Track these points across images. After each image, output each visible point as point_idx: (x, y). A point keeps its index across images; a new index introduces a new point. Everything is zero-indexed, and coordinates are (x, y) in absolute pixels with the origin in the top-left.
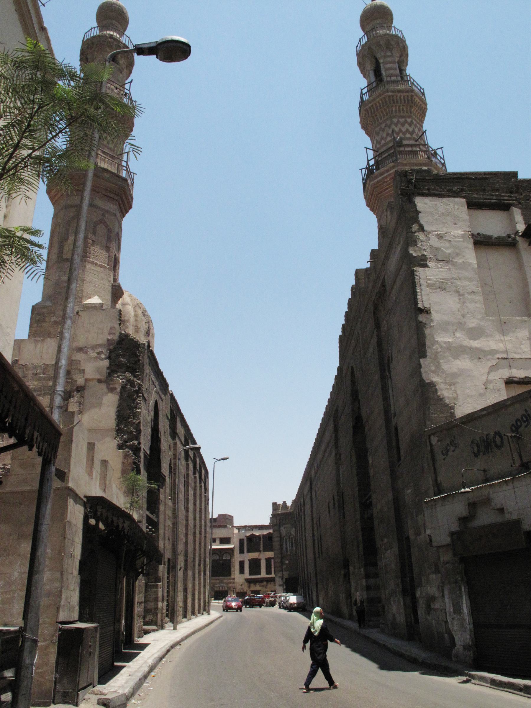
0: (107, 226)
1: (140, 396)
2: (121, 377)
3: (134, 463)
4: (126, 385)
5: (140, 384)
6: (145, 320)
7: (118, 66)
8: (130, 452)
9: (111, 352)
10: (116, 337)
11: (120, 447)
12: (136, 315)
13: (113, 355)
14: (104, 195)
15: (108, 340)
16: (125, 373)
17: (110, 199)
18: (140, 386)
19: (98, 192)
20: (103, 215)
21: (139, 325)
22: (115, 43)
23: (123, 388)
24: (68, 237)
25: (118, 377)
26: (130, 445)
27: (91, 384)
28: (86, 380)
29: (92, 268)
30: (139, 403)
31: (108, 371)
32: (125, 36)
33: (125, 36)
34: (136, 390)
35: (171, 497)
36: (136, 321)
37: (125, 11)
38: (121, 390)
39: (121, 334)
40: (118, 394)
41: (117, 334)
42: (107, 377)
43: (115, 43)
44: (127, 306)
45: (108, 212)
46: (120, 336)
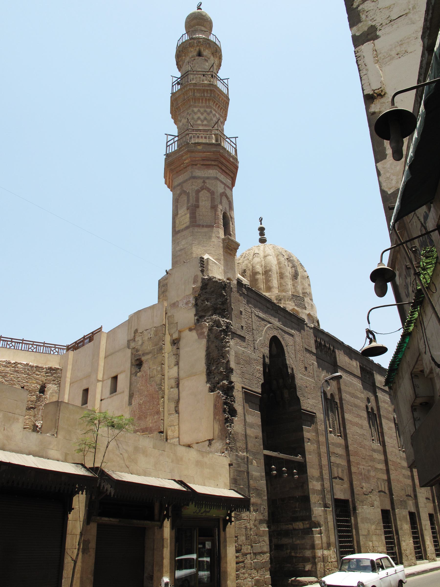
0: (209, 190)
1: (229, 334)
2: (207, 321)
3: (225, 403)
4: (213, 326)
5: (228, 323)
6: (291, 265)
7: (203, 58)
8: (221, 393)
9: (196, 299)
10: (199, 284)
11: (212, 390)
12: (279, 263)
13: (199, 302)
14: (202, 165)
15: (193, 288)
16: (212, 315)
17: (208, 166)
18: (228, 325)
19: (196, 165)
20: (204, 182)
21: (283, 271)
22: (195, 42)
23: (210, 330)
24: (178, 212)
25: (205, 321)
26: (221, 386)
27: (184, 334)
28: (180, 332)
29: (199, 230)
30: (228, 342)
31: (196, 318)
32: (212, 35)
33: (212, 35)
34: (224, 329)
35: (340, 433)
36: (280, 268)
37: (204, 14)
38: (208, 333)
39: (203, 279)
40: (205, 338)
41: (200, 280)
42: (195, 324)
43: (195, 42)
44: (268, 257)
45: (208, 178)
46: (202, 281)
